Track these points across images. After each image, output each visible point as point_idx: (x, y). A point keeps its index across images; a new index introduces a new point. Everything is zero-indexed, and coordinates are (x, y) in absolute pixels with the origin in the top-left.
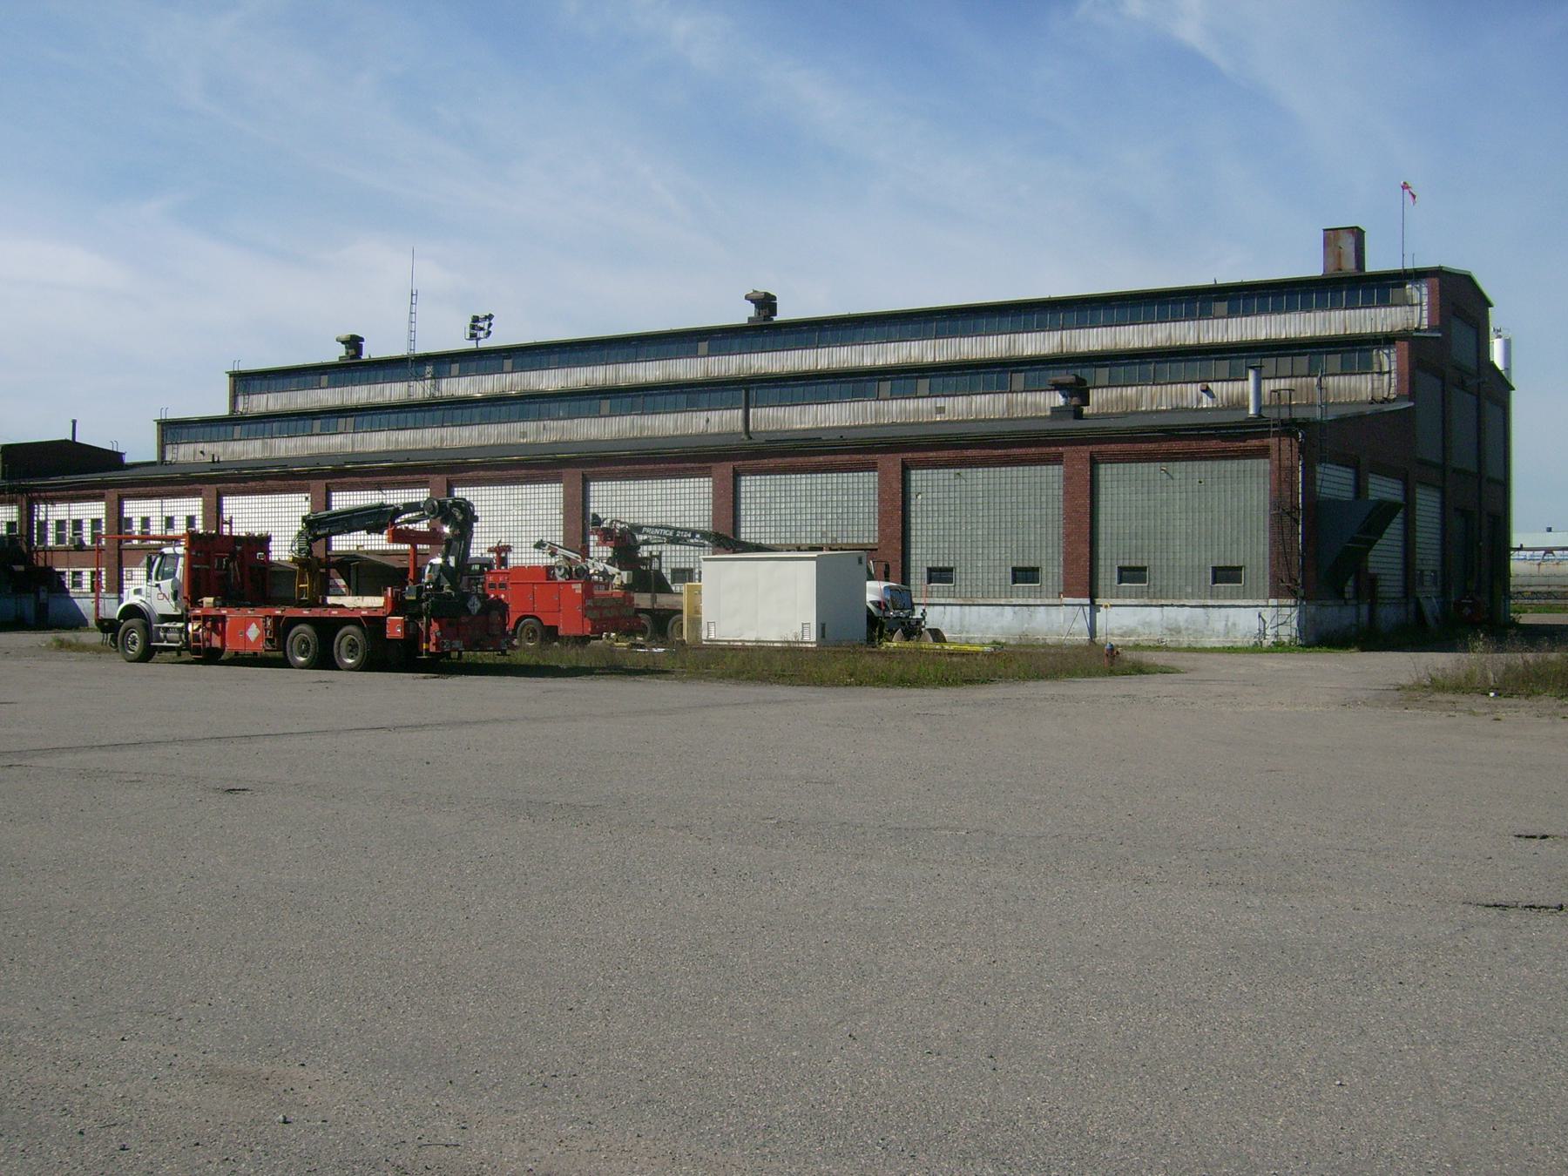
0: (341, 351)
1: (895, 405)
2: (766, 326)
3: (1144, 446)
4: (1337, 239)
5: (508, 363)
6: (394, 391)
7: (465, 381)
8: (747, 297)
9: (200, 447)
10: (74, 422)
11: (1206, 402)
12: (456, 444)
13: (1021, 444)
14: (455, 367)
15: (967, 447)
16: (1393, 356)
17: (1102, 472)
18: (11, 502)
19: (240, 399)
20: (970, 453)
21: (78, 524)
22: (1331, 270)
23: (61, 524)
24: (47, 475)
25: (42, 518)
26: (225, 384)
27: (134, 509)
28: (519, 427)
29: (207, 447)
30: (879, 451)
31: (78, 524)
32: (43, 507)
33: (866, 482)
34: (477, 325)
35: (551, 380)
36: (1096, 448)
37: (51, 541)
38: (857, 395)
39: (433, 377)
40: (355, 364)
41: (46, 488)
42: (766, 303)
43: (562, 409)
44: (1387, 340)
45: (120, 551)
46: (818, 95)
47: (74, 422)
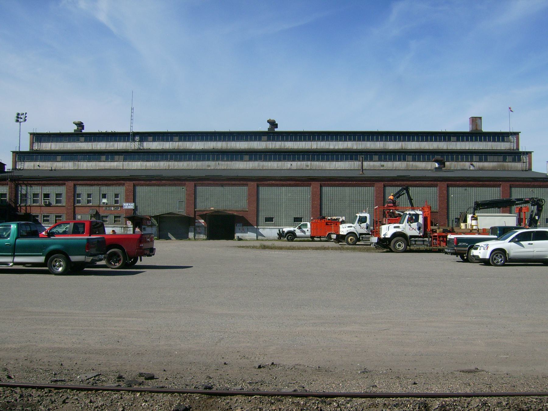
0: (76, 127)
3: (526, 183)
4: (476, 120)
8: (74, 123)
11: (472, 168)
15: (470, 181)
16: (527, 158)
17: (387, 190)
20: (471, 183)
22: (474, 129)
25: (24, 192)
26: (28, 137)
30: (439, 181)
32: (24, 187)
33: (434, 191)
34: (475, 121)
39: (140, 141)
42: (80, 125)
45: (74, 207)
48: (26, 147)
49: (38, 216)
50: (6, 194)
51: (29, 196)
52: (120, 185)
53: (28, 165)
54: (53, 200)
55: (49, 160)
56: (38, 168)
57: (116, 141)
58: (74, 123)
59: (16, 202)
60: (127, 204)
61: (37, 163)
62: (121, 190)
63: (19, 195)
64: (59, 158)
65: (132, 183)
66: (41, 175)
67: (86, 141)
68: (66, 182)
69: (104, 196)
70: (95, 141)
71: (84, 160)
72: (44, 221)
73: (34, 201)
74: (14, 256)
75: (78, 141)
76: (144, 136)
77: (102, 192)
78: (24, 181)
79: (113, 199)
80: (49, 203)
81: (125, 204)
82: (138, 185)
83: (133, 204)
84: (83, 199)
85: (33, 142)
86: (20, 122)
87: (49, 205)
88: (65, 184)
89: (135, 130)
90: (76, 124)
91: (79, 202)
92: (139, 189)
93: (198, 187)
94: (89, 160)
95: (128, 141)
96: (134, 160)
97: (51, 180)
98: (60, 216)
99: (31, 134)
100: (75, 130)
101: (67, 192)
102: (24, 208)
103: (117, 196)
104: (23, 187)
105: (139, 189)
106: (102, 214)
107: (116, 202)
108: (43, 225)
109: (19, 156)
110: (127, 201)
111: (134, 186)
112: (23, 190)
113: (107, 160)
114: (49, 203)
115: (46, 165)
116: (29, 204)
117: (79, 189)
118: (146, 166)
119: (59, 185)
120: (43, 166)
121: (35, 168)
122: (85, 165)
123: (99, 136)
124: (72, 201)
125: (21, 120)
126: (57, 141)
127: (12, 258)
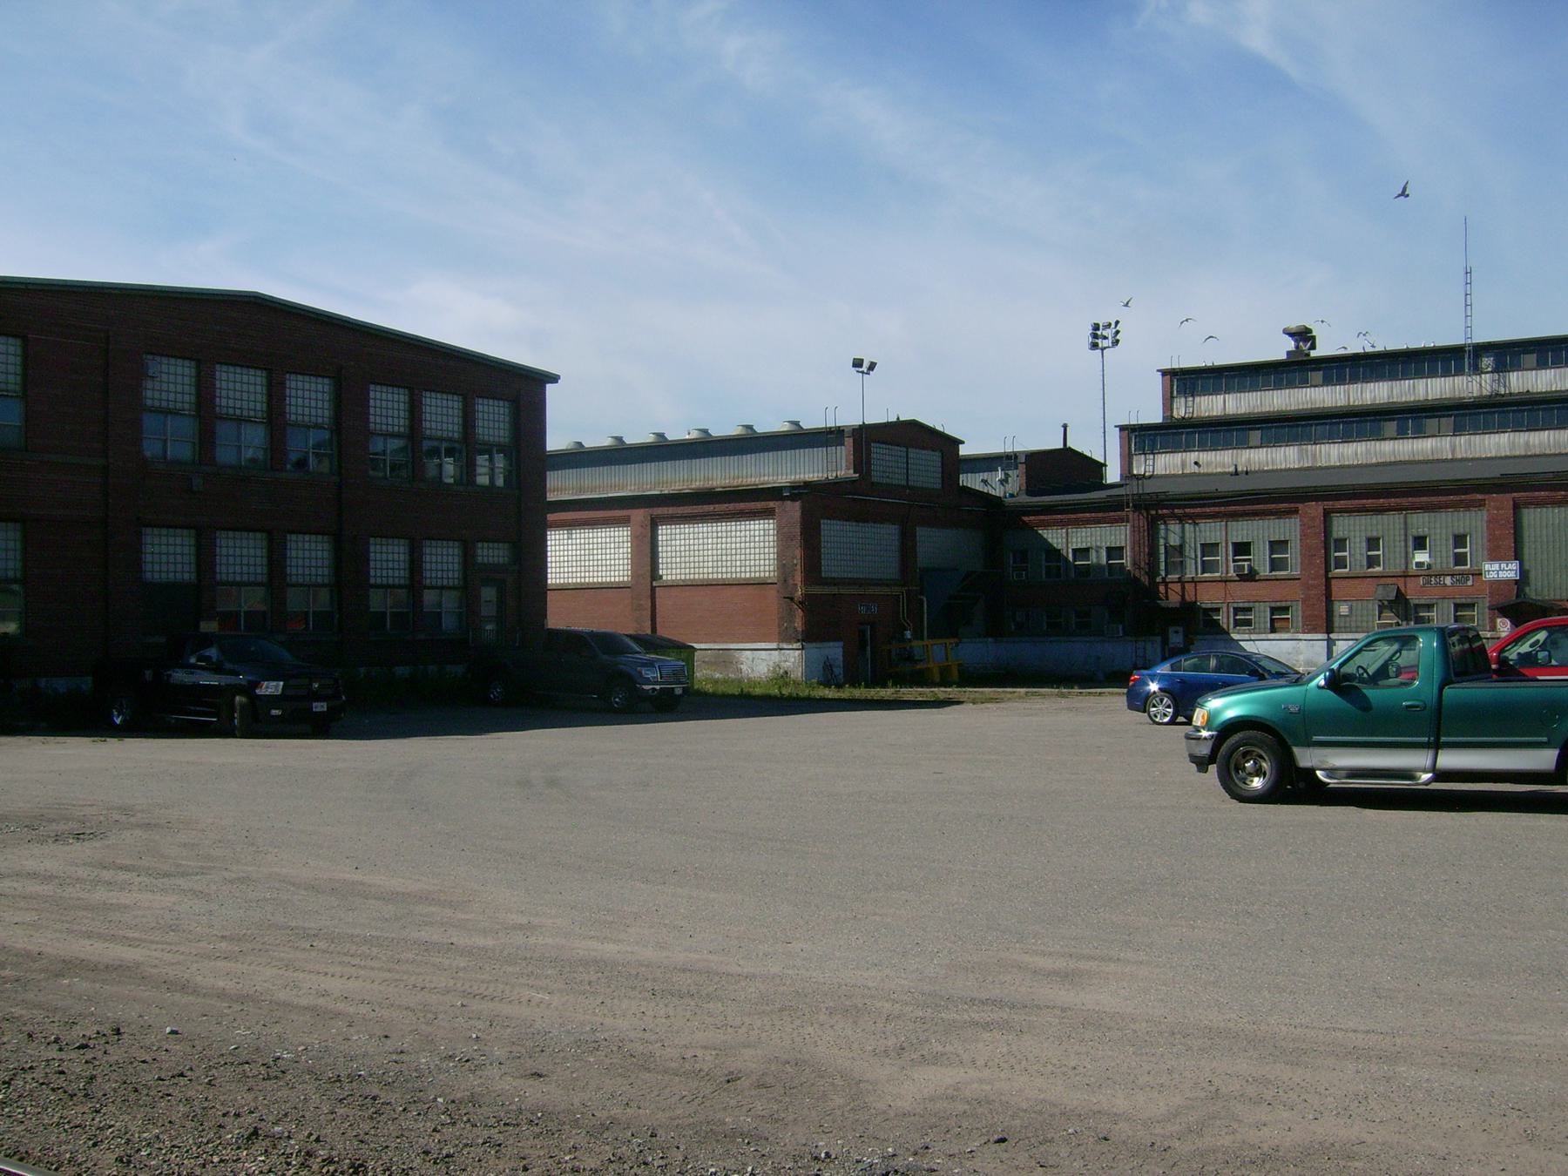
2: (1302, 365)
8: (1286, 332)
9: (1193, 456)
10: (1065, 427)
25: (1174, 540)
26: (1157, 382)
32: (1175, 527)
42: (1303, 335)
45: (1328, 581)
46: (874, 113)
47: (1065, 427)
48: (1153, 414)
49: (1217, 610)
50: (1121, 548)
51: (1189, 552)
52: (1468, 506)
53: (1167, 464)
54: (1260, 559)
55: (1227, 446)
56: (1195, 469)
57: (1419, 374)
58: (1286, 332)
59: (1152, 569)
60: (1496, 566)
61: (1193, 456)
62: (1474, 522)
63: (1162, 550)
64: (1255, 436)
65: (1507, 499)
66: (1208, 487)
67: (1327, 381)
68: (1300, 506)
69: (1420, 543)
70: (1354, 379)
71: (1331, 438)
72: (1237, 623)
73: (1206, 567)
74: (1436, 746)
75: (1305, 383)
76: (1508, 354)
77: (1413, 532)
78: (1173, 507)
79: (1448, 551)
80: (1251, 568)
81: (1487, 567)
82: (1528, 504)
83: (1514, 565)
84: (1354, 554)
85: (1172, 397)
86: (1103, 349)
87: (1250, 577)
88: (1296, 511)
89: (1482, 336)
90: (1291, 335)
91: (1341, 563)
92: (1531, 516)
93: (1525, 511)
94: (1347, 438)
95: (1459, 372)
96: (1488, 429)
97: (1258, 502)
98: (1285, 609)
99: (1164, 373)
100: (1289, 353)
101: (1304, 535)
102: (1177, 587)
103: (1459, 540)
104: (1171, 527)
105: (1531, 516)
106: (1414, 598)
107: (1460, 559)
108: (1235, 636)
109: (1140, 437)
110: (1495, 556)
111: (1516, 507)
112: (1172, 533)
113: (1401, 434)
114: (1251, 568)
115: (1218, 461)
116: (1189, 575)
117: (1342, 526)
118: (1527, 444)
119: (1279, 514)
120: (1209, 464)
121: (1187, 471)
122: (1336, 454)
123: (1268, 374)
124: (1319, 561)
125: (1105, 343)
126: (1242, 389)
127: (1431, 753)
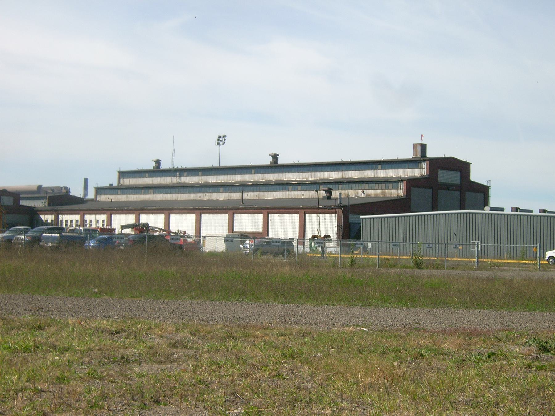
1: (293, 193)
2: (275, 166)
5: (200, 173)
6: (167, 180)
7: (188, 178)
9: (108, 196)
11: (363, 195)
12: (182, 199)
13: (291, 209)
14: (186, 173)
18: (52, 214)
19: (121, 180)
21: (72, 221)
23: (67, 221)
24: (61, 205)
26: (117, 175)
27: (88, 217)
28: (199, 195)
29: (110, 197)
31: (72, 221)
35: (213, 179)
36: (269, 211)
37: (64, 226)
38: (284, 190)
40: (157, 170)
41: (62, 210)
43: (210, 189)
44: (399, 180)
